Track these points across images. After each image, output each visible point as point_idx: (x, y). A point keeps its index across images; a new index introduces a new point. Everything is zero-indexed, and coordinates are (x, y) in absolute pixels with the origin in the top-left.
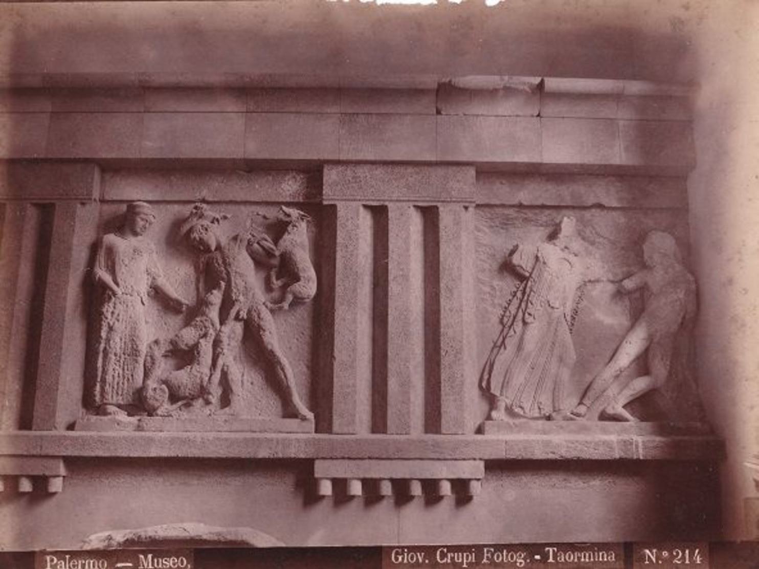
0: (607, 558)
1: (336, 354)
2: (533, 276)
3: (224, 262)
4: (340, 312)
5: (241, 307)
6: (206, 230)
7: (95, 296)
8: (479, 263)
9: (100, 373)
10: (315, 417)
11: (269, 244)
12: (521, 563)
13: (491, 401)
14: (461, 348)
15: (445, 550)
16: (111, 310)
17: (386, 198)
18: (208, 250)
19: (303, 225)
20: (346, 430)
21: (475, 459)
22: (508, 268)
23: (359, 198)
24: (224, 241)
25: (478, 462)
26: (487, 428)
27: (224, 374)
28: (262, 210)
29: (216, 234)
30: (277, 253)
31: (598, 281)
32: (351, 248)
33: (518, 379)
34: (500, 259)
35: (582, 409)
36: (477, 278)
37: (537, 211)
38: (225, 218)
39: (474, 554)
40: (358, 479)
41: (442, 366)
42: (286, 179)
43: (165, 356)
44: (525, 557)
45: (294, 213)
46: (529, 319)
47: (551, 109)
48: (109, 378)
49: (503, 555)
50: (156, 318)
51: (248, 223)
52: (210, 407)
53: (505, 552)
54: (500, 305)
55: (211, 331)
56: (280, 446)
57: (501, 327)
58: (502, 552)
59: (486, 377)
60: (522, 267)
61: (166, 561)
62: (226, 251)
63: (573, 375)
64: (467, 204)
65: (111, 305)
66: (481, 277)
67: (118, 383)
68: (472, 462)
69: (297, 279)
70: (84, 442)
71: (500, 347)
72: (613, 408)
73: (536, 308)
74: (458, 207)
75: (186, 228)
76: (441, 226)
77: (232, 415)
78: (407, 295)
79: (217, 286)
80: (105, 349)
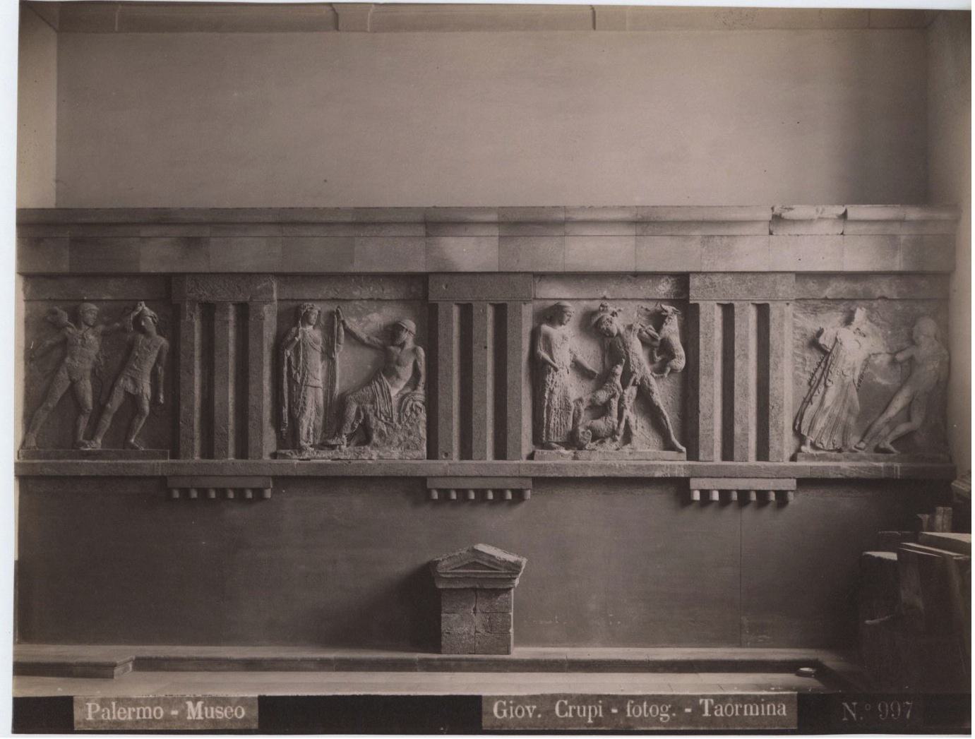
0: (776, 712)
1: (701, 409)
2: (833, 352)
3: (624, 345)
4: (703, 381)
5: (638, 376)
6: (611, 322)
7: (539, 369)
8: (795, 341)
9: (545, 422)
10: (687, 450)
11: (653, 332)
12: (665, 718)
13: (801, 438)
14: (783, 404)
15: (566, 702)
16: (550, 380)
17: (732, 299)
18: (611, 335)
19: (675, 318)
20: (707, 459)
21: (790, 478)
22: (814, 343)
23: (714, 298)
24: (622, 330)
25: (792, 480)
26: (798, 457)
27: (627, 422)
28: (645, 305)
29: (617, 325)
30: (659, 339)
31: (880, 353)
32: (709, 335)
33: (820, 425)
34: (809, 335)
35: (862, 445)
36: (794, 353)
37: (837, 302)
38: (620, 310)
39: (600, 707)
40: (698, 490)
41: (770, 416)
42: (662, 281)
43: (585, 409)
44: (669, 709)
45: (670, 309)
46: (829, 384)
47: (850, 229)
48: (552, 425)
49: (643, 709)
50: (576, 382)
51: (636, 315)
52: (617, 443)
53: (645, 705)
54: (809, 372)
55: (618, 394)
56: (669, 470)
57: (809, 387)
58: (642, 705)
59: (798, 423)
60: (825, 346)
61: (220, 710)
62: (625, 337)
63: (857, 421)
64: (788, 302)
65: (551, 376)
66: (795, 351)
67: (557, 428)
68: (788, 480)
69: (673, 357)
70: (544, 467)
71: (808, 402)
72: (884, 444)
73: (835, 377)
74: (783, 304)
75: (596, 319)
76: (771, 318)
77: (632, 449)
78: (747, 370)
79: (619, 362)
80: (548, 405)
